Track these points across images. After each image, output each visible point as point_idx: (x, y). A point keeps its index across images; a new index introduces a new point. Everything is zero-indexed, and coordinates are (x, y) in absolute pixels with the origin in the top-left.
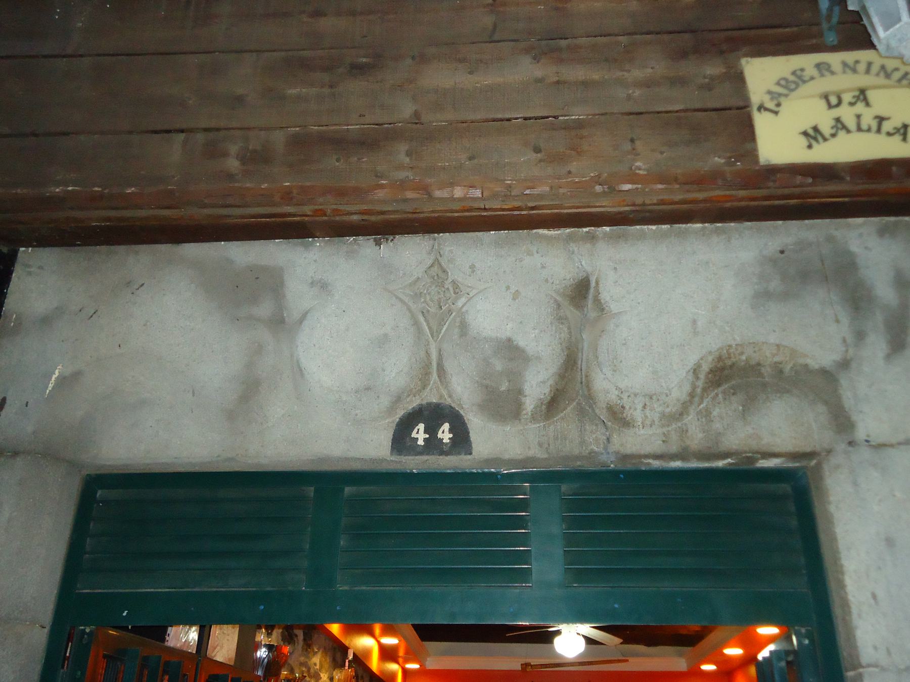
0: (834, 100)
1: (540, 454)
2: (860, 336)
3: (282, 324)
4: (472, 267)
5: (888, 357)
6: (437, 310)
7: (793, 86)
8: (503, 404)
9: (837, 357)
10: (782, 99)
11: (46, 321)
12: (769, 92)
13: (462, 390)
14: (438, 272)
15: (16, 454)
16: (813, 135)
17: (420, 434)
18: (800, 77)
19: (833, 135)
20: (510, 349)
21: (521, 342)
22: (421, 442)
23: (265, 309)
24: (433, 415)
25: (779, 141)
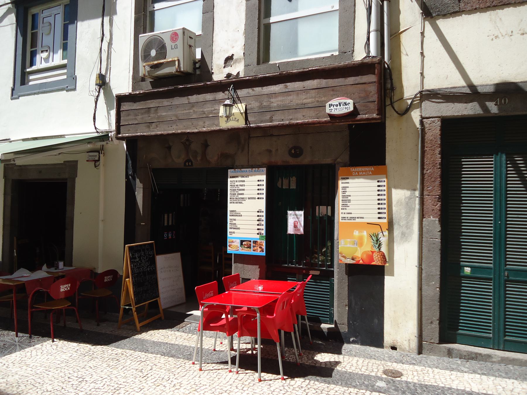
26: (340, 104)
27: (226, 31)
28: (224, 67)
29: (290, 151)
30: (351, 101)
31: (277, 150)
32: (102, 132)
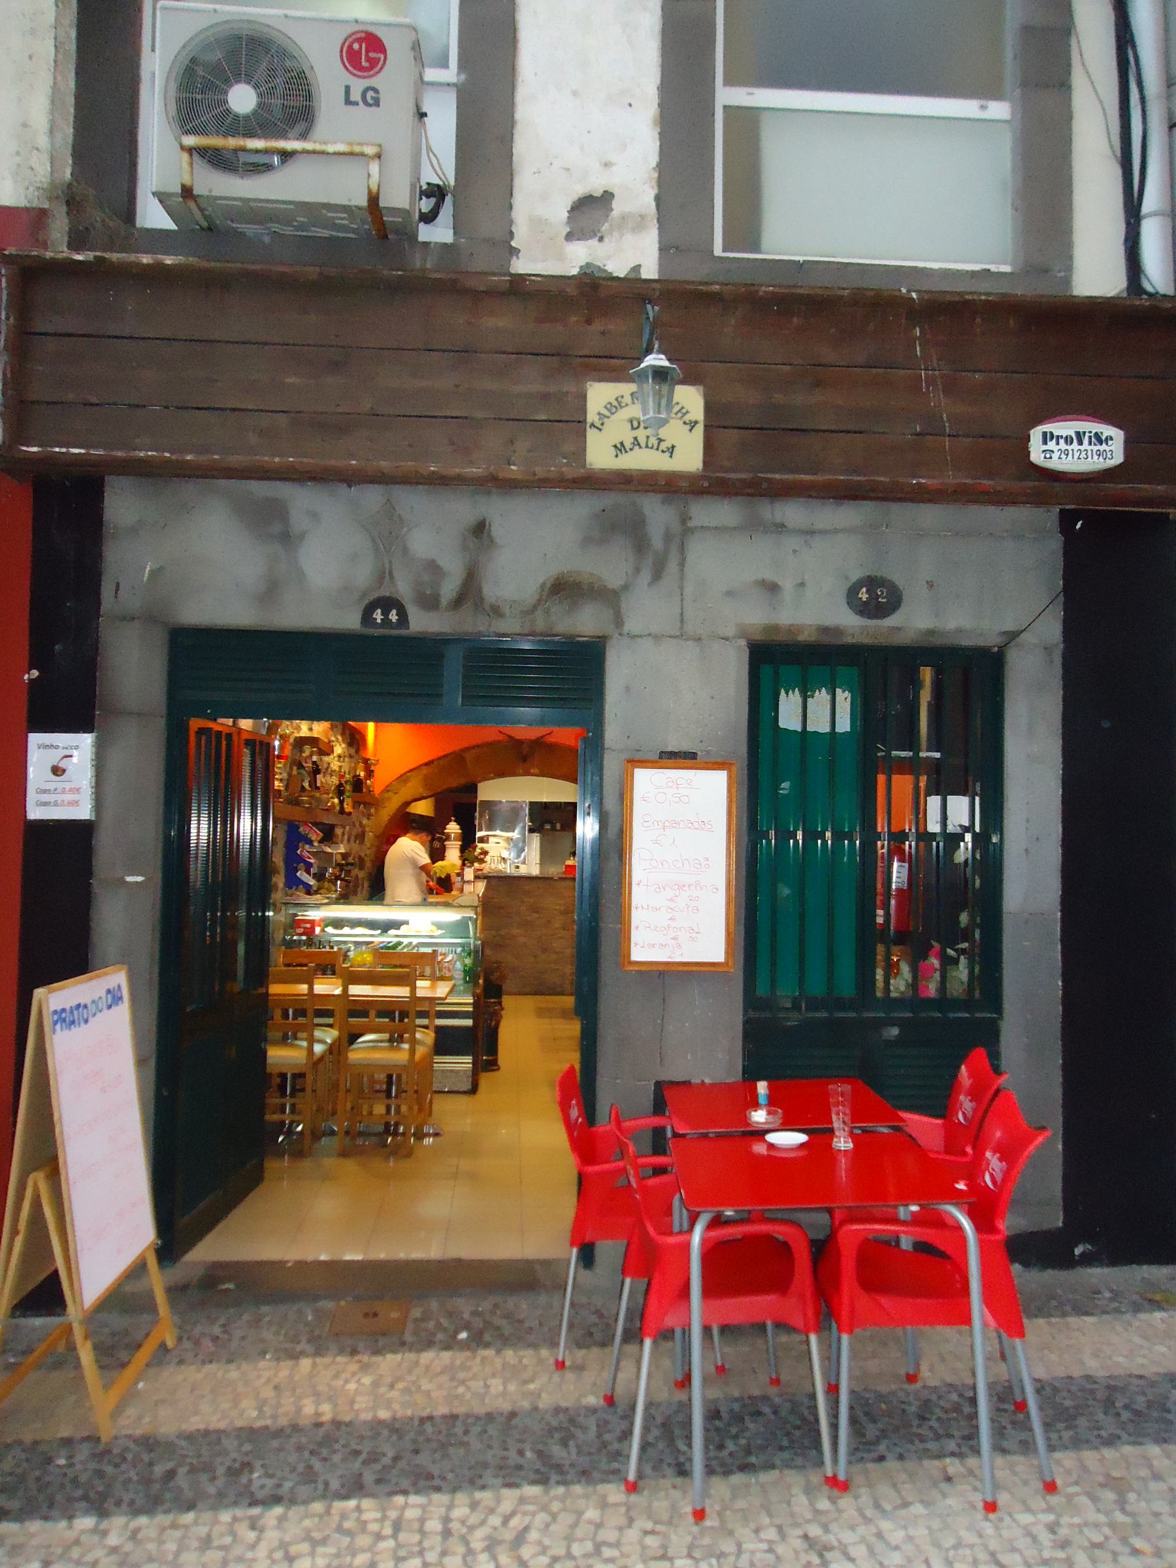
0: (635, 424)
1: (449, 631)
2: (637, 570)
3: (288, 539)
4: (412, 507)
5: (650, 585)
6: (387, 536)
7: (614, 410)
8: (430, 603)
9: (622, 582)
10: (606, 420)
11: (134, 530)
12: (599, 414)
13: (403, 588)
14: (389, 508)
15: (133, 619)
16: (620, 448)
17: (378, 616)
18: (619, 403)
19: (631, 450)
20: (433, 567)
21: (441, 563)
22: (379, 621)
23: (276, 528)
24: (387, 603)
25: (600, 454)
26: (1080, 436)
27: (575, 93)
28: (569, 237)
29: (852, 592)
30: (1116, 435)
31: (802, 584)
32: (455, 1176)
